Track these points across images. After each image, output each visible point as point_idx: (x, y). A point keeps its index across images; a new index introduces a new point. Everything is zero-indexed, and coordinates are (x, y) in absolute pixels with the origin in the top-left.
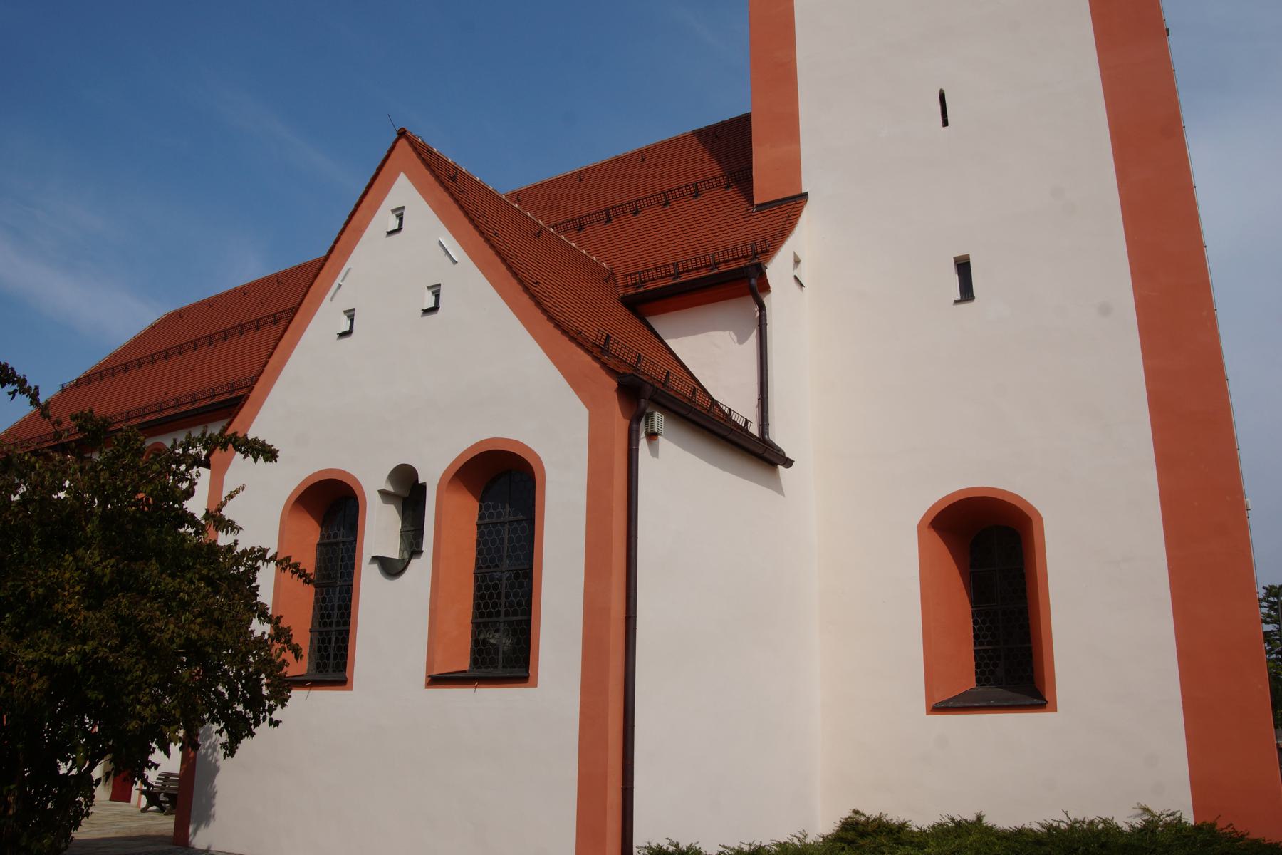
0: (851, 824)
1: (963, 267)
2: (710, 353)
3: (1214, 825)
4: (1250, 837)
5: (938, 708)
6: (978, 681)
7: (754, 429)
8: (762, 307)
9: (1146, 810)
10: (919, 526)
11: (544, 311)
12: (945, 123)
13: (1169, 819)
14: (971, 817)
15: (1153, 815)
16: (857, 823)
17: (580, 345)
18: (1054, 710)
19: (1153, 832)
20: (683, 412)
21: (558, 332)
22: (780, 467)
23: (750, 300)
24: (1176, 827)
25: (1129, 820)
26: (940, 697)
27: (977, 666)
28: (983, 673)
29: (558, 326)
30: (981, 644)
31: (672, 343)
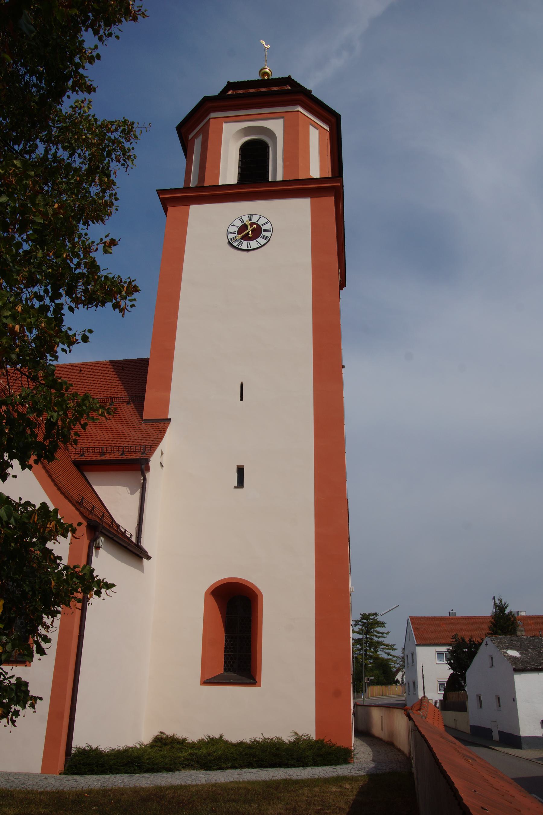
0: (158, 739)
1: (240, 471)
2: (116, 498)
3: (323, 740)
4: (337, 745)
5: (206, 682)
6: (225, 669)
7: (134, 539)
8: (145, 479)
9: (296, 733)
10: (206, 593)
11: (53, 480)
12: (242, 399)
13: (305, 738)
14: (218, 736)
15: (299, 736)
16: (162, 738)
17: (70, 501)
18: (260, 686)
19: (298, 743)
20: (111, 536)
21: (59, 493)
22: (144, 560)
23: (139, 473)
24: (308, 741)
25: (288, 738)
26: (207, 677)
27: (225, 662)
28: (227, 666)
29: (59, 489)
30: (228, 652)
31: (96, 488)
